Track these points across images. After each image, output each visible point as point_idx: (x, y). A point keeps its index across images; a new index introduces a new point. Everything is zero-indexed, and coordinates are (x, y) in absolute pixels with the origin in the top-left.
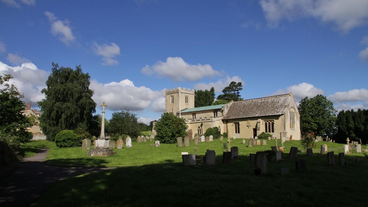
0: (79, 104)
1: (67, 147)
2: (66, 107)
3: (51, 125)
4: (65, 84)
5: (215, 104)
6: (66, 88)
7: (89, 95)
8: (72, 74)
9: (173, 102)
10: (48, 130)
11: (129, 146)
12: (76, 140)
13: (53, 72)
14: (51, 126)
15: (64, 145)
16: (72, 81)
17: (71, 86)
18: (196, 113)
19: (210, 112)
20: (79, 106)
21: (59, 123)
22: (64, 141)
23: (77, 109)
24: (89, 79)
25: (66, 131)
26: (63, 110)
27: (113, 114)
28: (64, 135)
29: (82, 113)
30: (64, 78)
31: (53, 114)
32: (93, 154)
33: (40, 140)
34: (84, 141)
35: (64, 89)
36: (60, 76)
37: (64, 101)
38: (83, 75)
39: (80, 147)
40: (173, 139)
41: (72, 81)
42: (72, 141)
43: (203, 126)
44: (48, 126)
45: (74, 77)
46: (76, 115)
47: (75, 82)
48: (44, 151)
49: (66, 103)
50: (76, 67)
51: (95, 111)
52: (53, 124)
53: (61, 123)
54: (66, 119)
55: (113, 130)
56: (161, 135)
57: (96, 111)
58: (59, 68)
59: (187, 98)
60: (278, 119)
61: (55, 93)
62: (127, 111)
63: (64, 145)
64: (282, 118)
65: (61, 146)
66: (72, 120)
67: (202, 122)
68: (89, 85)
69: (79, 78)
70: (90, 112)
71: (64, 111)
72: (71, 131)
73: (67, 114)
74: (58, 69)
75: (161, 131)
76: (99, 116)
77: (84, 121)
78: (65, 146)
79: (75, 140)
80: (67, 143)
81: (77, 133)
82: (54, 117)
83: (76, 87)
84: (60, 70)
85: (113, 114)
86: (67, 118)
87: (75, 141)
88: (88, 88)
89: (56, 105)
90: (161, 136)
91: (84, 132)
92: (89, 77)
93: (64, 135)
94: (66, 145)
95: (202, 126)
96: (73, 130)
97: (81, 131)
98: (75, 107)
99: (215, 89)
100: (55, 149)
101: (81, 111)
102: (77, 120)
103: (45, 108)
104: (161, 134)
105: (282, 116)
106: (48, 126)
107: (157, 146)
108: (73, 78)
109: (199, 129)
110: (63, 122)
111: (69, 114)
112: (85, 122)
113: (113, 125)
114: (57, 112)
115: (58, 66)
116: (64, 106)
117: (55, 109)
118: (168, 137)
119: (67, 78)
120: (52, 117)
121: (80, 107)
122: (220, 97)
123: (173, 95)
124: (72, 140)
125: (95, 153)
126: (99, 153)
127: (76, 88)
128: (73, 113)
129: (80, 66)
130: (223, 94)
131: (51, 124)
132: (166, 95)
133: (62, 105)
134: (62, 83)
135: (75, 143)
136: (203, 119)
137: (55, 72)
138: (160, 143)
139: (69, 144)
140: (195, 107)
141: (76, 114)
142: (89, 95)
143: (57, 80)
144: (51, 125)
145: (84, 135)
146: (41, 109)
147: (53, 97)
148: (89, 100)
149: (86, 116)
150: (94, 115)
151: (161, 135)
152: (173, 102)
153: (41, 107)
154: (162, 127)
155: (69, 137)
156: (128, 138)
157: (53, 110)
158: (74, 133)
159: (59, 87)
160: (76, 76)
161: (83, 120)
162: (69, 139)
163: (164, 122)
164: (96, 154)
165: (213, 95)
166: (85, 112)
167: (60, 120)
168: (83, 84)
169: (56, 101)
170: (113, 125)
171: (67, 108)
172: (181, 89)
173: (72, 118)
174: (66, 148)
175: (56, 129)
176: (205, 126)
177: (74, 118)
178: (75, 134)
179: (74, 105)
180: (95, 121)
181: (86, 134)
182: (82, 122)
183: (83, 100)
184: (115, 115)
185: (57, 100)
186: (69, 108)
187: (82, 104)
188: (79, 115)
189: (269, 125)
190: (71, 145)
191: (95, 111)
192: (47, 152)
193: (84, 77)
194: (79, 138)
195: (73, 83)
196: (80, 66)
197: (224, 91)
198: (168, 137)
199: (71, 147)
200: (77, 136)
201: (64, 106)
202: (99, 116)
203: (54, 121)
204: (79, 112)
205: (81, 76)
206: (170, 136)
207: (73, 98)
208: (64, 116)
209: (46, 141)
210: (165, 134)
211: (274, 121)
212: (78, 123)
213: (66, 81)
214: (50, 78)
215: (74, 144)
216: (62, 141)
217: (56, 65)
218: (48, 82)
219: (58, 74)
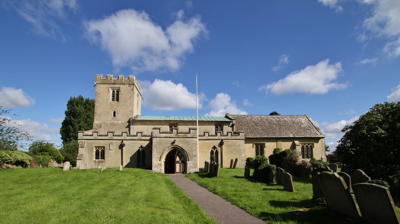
18: (179, 123)
60: (317, 142)
64: (322, 142)
67: (222, 140)
105: (322, 139)
152: (118, 100)
176: (228, 146)
189: (307, 149)
211: (313, 144)
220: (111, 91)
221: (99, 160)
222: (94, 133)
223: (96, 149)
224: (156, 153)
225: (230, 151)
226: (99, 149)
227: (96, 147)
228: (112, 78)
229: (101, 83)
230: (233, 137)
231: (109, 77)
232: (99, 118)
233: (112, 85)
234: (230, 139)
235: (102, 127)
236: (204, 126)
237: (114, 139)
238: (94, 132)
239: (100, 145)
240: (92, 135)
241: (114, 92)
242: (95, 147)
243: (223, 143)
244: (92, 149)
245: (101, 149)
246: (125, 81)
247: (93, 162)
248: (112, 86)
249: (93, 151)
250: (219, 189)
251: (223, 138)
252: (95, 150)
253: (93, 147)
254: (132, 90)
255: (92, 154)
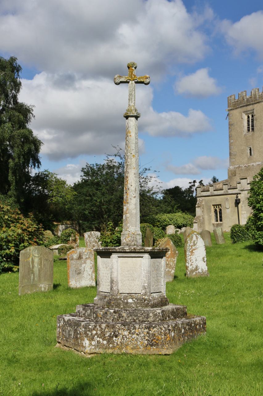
11: (197, 268)
27: (83, 169)
34: (27, 256)
43: (240, 205)
51: (37, 162)
55: (87, 212)
57: (41, 160)
62: (120, 161)
68: (18, 91)
76: (47, 176)
85: (83, 169)
88: (15, 97)
92: (18, 69)
95: (238, 203)
97: (6, 217)
109: (218, 210)
113: (87, 198)
123: (250, 108)
125: (102, 336)
126: (126, 333)
132: (229, 110)
148: (22, 131)
149: (14, 173)
150: (33, 172)
152: (253, 129)
156: (194, 238)
164: (111, 337)
181: (24, 227)
191: (39, 162)
202: (47, 176)
220: (245, 117)
222: (237, 184)
223: (214, 207)
224: (245, 212)
226: (217, 207)
227: (213, 205)
229: (232, 108)
232: (234, 161)
233: (245, 107)
235: (237, 175)
237: (202, 195)
238: (224, 185)
239: (216, 203)
240: (222, 190)
241: (248, 117)
244: (210, 209)
245: (219, 207)
246: (259, 98)
248: (245, 109)
249: (210, 211)
250: (127, 248)
252: (213, 209)
253: (210, 206)
255: (211, 215)
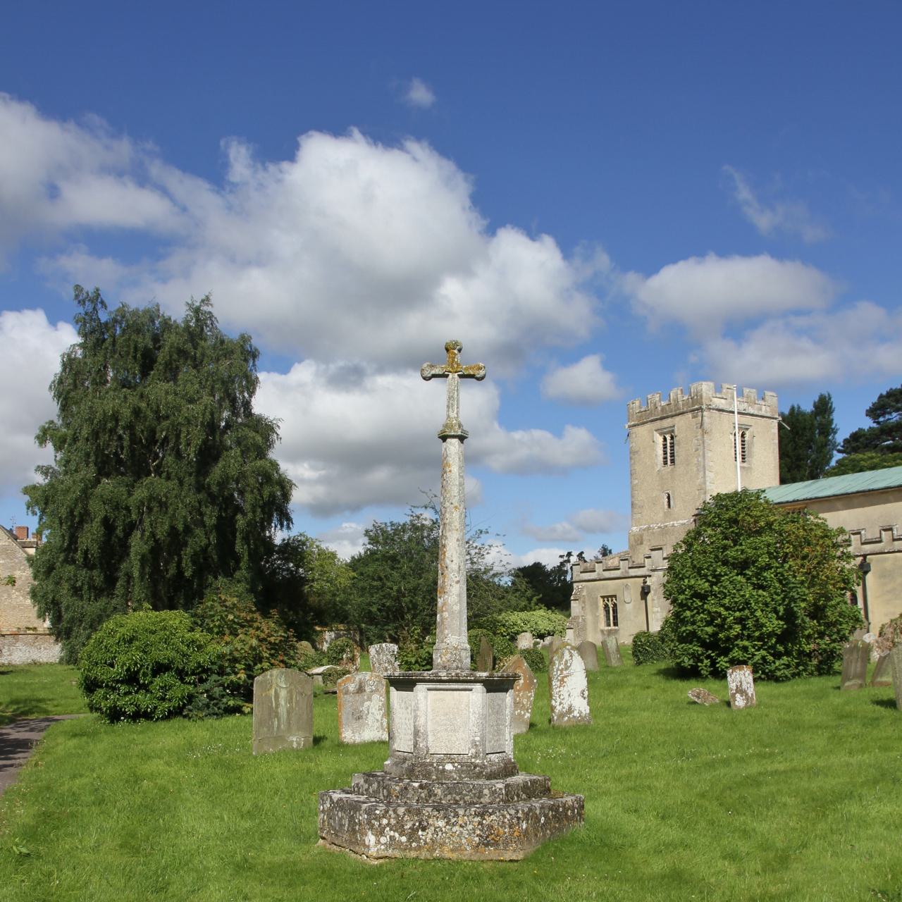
0: (209, 485)
1: (148, 716)
2: (151, 498)
3: (81, 589)
4: (139, 389)
5: (842, 469)
6: (143, 405)
7: (253, 438)
8: (170, 340)
9: (670, 457)
10: (66, 616)
11: (570, 710)
12: (205, 671)
13: (85, 336)
14: (81, 597)
15: (130, 710)
16: (172, 372)
17: (167, 393)
19: (884, 503)
20: (210, 495)
21: (116, 579)
22: (132, 679)
23: (203, 509)
24: (254, 365)
25: (141, 618)
26: (134, 517)
28: (131, 641)
29: (225, 528)
30: (135, 357)
31: (90, 537)
32: (381, 833)
33: (35, 663)
34: (267, 686)
35: (137, 412)
36: (114, 352)
37: (140, 471)
38: (222, 342)
39: (231, 720)
40: (788, 653)
41: (172, 372)
42: (182, 680)
43: (869, 577)
44: (66, 599)
45: (182, 353)
46: (199, 539)
47: (186, 372)
48: (57, 720)
49: (146, 481)
50: (190, 305)
51: (285, 518)
52: (92, 587)
53: (129, 577)
54: (155, 554)
56: (709, 630)
57: (292, 516)
58: (111, 312)
59: (743, 436)
61: (95, 435)
63: (133, 708)
65: (115, 715)
66: (179, 563)
67: (865, 556)
68: (252, 394)
69: (203, 355)
70: (265, 523)
71: (141, 521)
72: (176, 619)
73: (153, 535)
74: (104, 317)
75: (711, 605)
76: (304, 544)
77: (237, 568)
78: (138, 715)
79: (202, 672)
80: (148, 691)
81: (210, 630)
82: (95, 550)
83: (191, 401)
84: (115, 321)
86: (156, 551)
87: (202, 681)
88: (247, 405)
89: (99, 490)
90: (715, 635)
91: (252, 620)
93: (131, 641)
94: (143, 707)
95: (866, 573)
96: (186, 609)
97: (231, 617)
98: (191, 498)
99: (836, 403)
100: (75, 735)
101: (219, 518)
102: (204, 566)
103: (51, 507)
104: (709, 623)
106: (66, 599)
107: (740, 702)
108: (175, 356)
109: (611, 606)
110: (136, 574)
111: (162, 531)
112: (242, 573)
113: (375, 583)
114: (108, 525)
115: (102, 302)
116: (140, 493)
117: (98, 510)
118: (760, 639)
119: (147, 362)
120: (86, 553)
121: (212, 498)
122: (858, 441)
123: (667, 423)
124: (181, 674)
125: (399, 827)
126: (441, 823)
127: (191, 406)
128: (180, 527)
129: (206, 300)
130: (867, 424)
131: (79, 584)
133: (130, 494)
134: (125, 384)
135: (201, 688)
136: (867, 535)
137: (92, 332)
138: (755, 680)
139: (163, 699)
140: (783, 481)
141: (198, 531)
142: (253, 438)
143: (102, 373)
144: (81, 589)
145: (254, 642)
146: (41, 519)
147: (88, 455)
149: (246, 539)
150: (279, 536)
151: (709, 630)
152: (673, 461)
153: (36, 510)
154: (718, 577)
155: (163, 654)
157: (85, 516)
158: (192, 630)
159: (111, 402)
160: (189, 346)
161: (232, 564)
162: (159, 669)
163: (725, 548)
164: (414, 830)
165: (827, 429)
166: (241, 522)
167: (123, 566)
168: (227, 383)
169: (103, 472)
170: (375, 583)
171: (154, 504)
172: (711, 393)
173: (179, 556)
174: (143, 723)
175: (104, 610)
176: (884, 575)
177: (188, 551)
178: (197, 635)
179: (186, 487)
180: (288, 569)
181: (262, 635)
182: (229, 574)
183: (230, 463)
184: (377, 536)
185: (105, 467)
186: (163, 505)
187: (223, 484)
188: (213, 539)
190: (175, 703)
191: (289, 520)
192: (32, 756)
193: (228, 354)
194: (221, 656)
195: (175, 379)
196: (206, 300)
197: (875, 412)
198: (760, 639)
199: (177, 722)
200: (209, 648)
201: (140, 493)
202: (304, 544)
203: (95, 573)
204: (211, 520)
205: (214, 347)
206: (770, 635)
207: (179, 455)
208: (138, 545)
209: (60, 668)
210: (740, 621)
212: (210, 578)
213: (145, 374)
214: (69, 363)
215: (191, 698)
216: (122, 682)
217: (92, 301)
218: (61, 382)
219: (104, 340)
221: (610, 628)
222: (883, 532)
225: (888, 592)
226: (608, 601)
228: (658, 404)
230: (896, 543)
231: (651, 402)
234: (889, 553)
235: (645, 543)
236: (883, 506)
241: (665, 439)
242: (602, 597)
243: (869, 565)
245: (612, 600)
247: (600, 633)
248: (658, 424)
249: (597, 608)
250: (443, 675)
251: (868, 548)
252: (601, 604)
253: (597, 598)
254: (699, 425)
255: (598, 614)
